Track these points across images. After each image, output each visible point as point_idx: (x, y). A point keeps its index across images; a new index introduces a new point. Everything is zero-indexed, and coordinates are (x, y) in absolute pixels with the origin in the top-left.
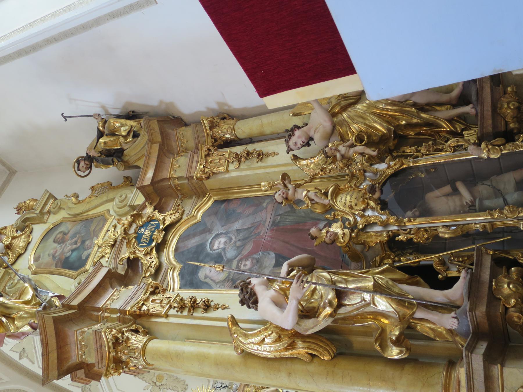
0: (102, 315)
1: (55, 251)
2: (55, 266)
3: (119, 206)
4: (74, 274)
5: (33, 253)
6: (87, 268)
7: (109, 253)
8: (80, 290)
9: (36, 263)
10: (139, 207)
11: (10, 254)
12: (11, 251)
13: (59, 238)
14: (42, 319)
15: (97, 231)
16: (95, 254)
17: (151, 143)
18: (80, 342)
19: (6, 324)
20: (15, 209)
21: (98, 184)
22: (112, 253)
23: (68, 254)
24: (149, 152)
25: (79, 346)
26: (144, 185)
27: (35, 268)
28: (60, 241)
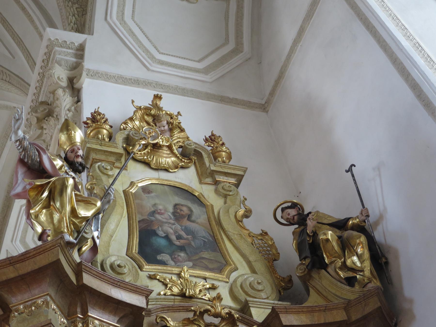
0: (78, 319)
1: (163, 211)
2: (141, 219)
3: (244, 286)
4: (134, 251)
5: (154, 182)
6: (146, 267)
7: (173, 293)
8: (106, 278)
9: (141, 191)
10: (248, 317)
11: (146, 151)
12: (151, 150)
13: (181, 210)
14: (54, 246)
15: (202, 262)
16: (168, 272)
17: (345, 307)
18: (35, 303)
19: (40, 199)
20: (212, 133)
21: (272, 239)
22: (173, 297)
23: (161, 233)
24: (332, 307)
25: (30, 302)
26: (281, 317)
27: (134, 192)
28: (178, 213)
